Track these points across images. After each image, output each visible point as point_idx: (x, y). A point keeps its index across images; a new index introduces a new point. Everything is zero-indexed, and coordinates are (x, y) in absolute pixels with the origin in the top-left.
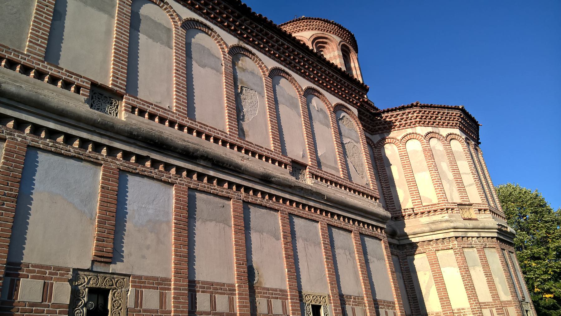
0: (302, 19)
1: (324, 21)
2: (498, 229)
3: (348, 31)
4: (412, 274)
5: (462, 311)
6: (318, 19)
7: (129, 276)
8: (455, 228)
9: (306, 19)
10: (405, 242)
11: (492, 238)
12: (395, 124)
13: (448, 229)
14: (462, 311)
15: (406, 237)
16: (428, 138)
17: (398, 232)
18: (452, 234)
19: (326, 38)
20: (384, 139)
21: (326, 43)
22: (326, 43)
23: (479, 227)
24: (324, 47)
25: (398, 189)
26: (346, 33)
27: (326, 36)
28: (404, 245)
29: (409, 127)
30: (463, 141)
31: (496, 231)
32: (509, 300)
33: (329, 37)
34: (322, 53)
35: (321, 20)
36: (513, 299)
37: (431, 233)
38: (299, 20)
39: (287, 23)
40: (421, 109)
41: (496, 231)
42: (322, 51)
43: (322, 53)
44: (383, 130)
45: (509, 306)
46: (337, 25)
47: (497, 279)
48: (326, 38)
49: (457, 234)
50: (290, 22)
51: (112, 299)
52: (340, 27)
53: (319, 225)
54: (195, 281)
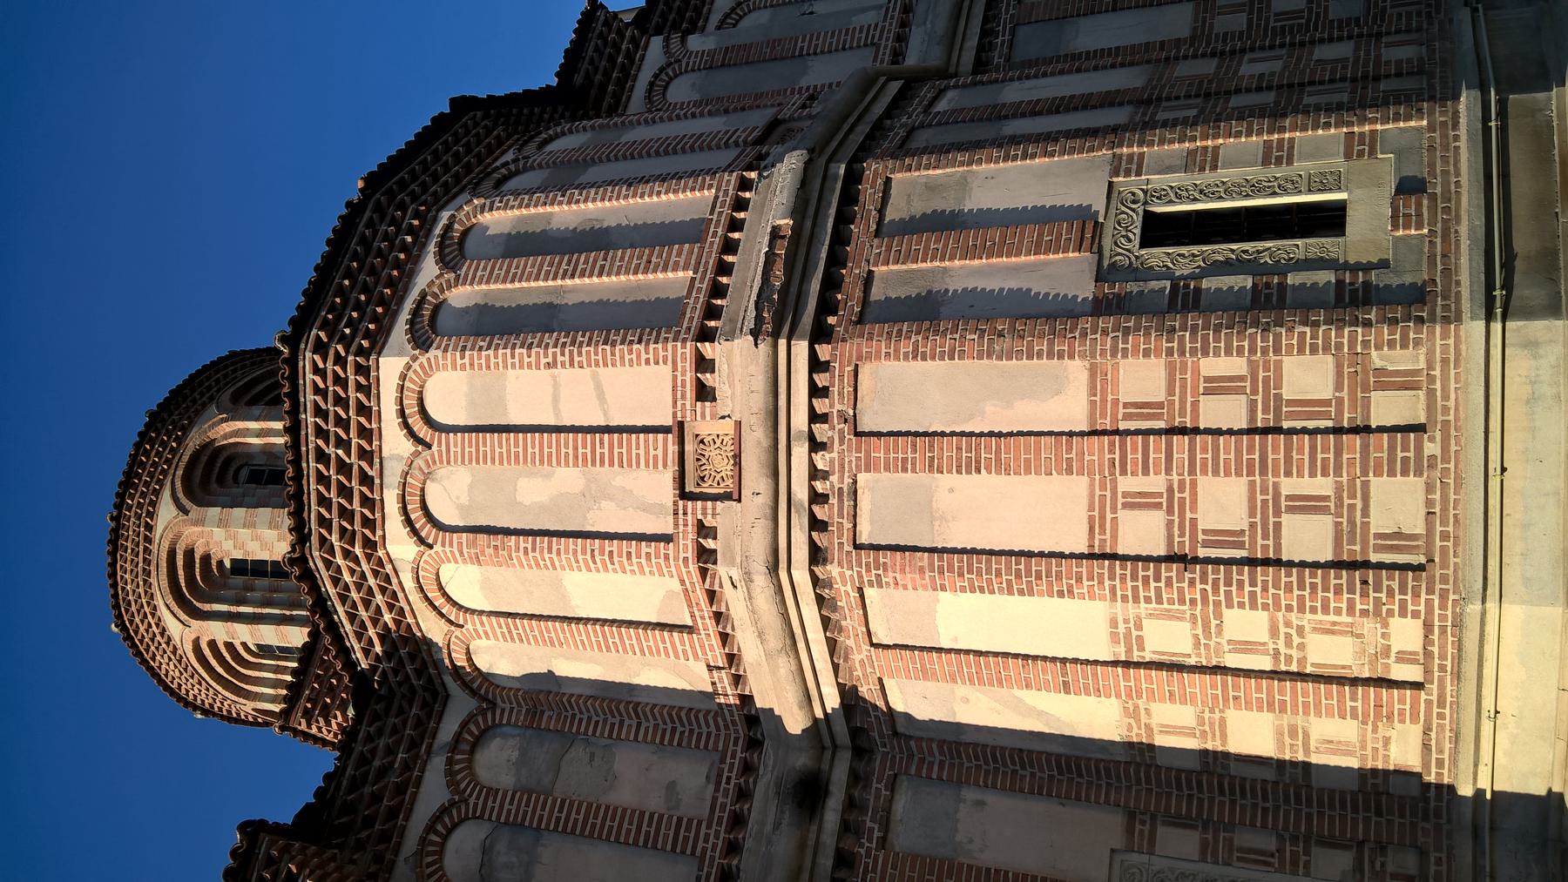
0: (124, 628)
1: (113, 554)
2: (776, 335)
3: (138, 446)
4: (967, 738)
5: (1122, 628)
6: (113, 575)
7: (1110, 184)
8: (773, 569)
9: (120, 616)
10: (841, 729)
11: (816, 365)
12: (391, 625)
13: (779, 590)
14: (1122, 628)
15: (823, 727)
16: (427, 531)
17: (802, 761)
18: (801, 576)
19: (172, 554)
20: (456, 671)
21: (189, 553)
22: (189, 553)
23: (766, 443)
24: (206, 558)
25: (635, 681)
26: (147, 453)
27: (164, 556)
28: (855, 733)
29: (394, 580)
30: (423, 359)
31: (782, 343)
32: (1084, 377)
33: (165, 545)
34: (228, 564)
35: (113, 564)
36: (1083, 356)
37: (801, 645)
38: (129, 638)
39: (150, 668)
40: (314, 539)
41: (782, 343)
42: (220, 563)
43: (228, 564)
44: (424, 662)
45: (1115, 391)
46: (121, 496)
47: (989, 408)
48: (172, 554)
49: (801, 553)
50: (144, 661)
51: (1171, 202)
52: (127, 484)
53: (897, 177)
54: (1095, 298)
